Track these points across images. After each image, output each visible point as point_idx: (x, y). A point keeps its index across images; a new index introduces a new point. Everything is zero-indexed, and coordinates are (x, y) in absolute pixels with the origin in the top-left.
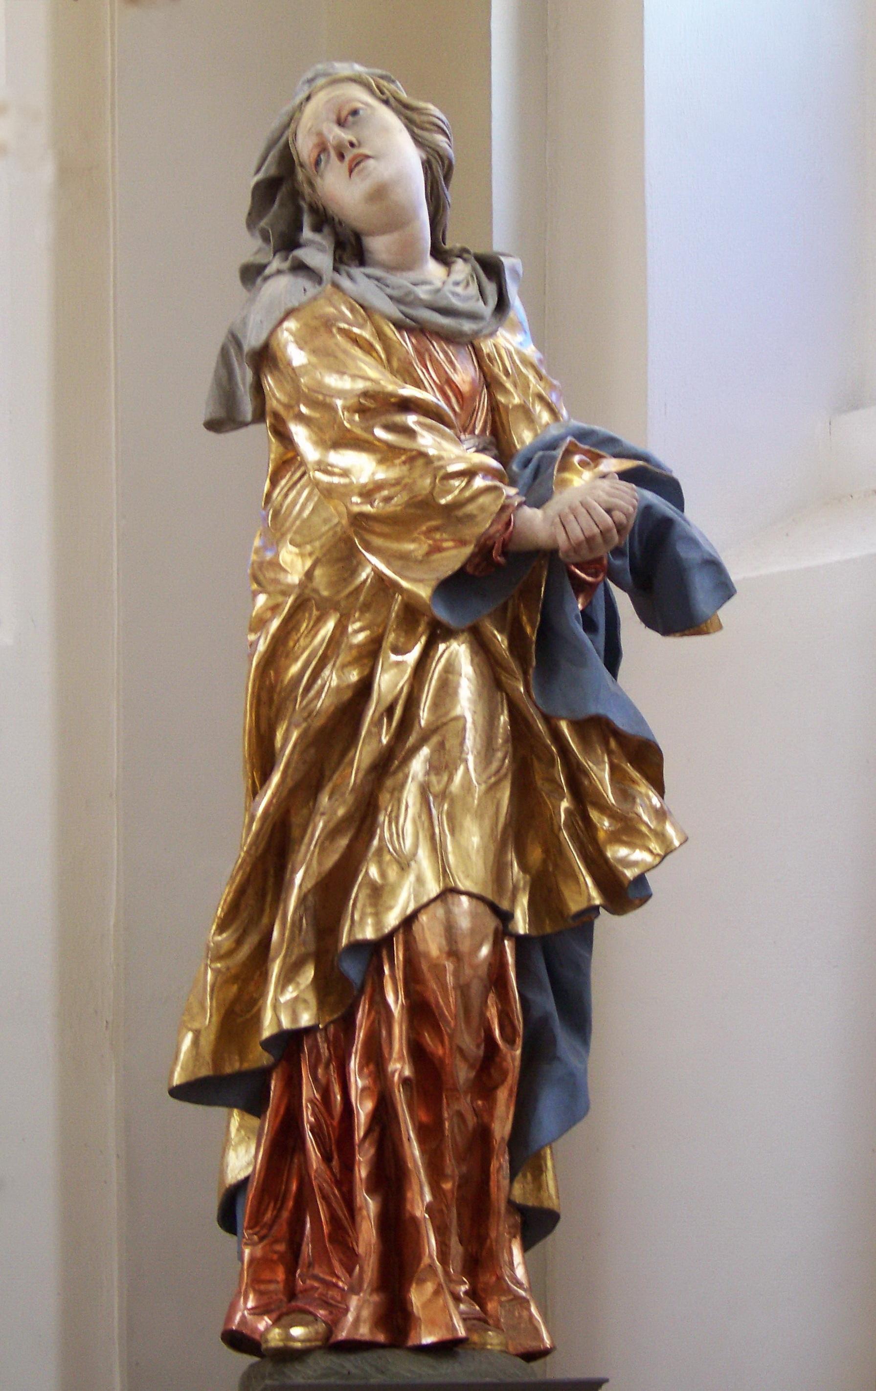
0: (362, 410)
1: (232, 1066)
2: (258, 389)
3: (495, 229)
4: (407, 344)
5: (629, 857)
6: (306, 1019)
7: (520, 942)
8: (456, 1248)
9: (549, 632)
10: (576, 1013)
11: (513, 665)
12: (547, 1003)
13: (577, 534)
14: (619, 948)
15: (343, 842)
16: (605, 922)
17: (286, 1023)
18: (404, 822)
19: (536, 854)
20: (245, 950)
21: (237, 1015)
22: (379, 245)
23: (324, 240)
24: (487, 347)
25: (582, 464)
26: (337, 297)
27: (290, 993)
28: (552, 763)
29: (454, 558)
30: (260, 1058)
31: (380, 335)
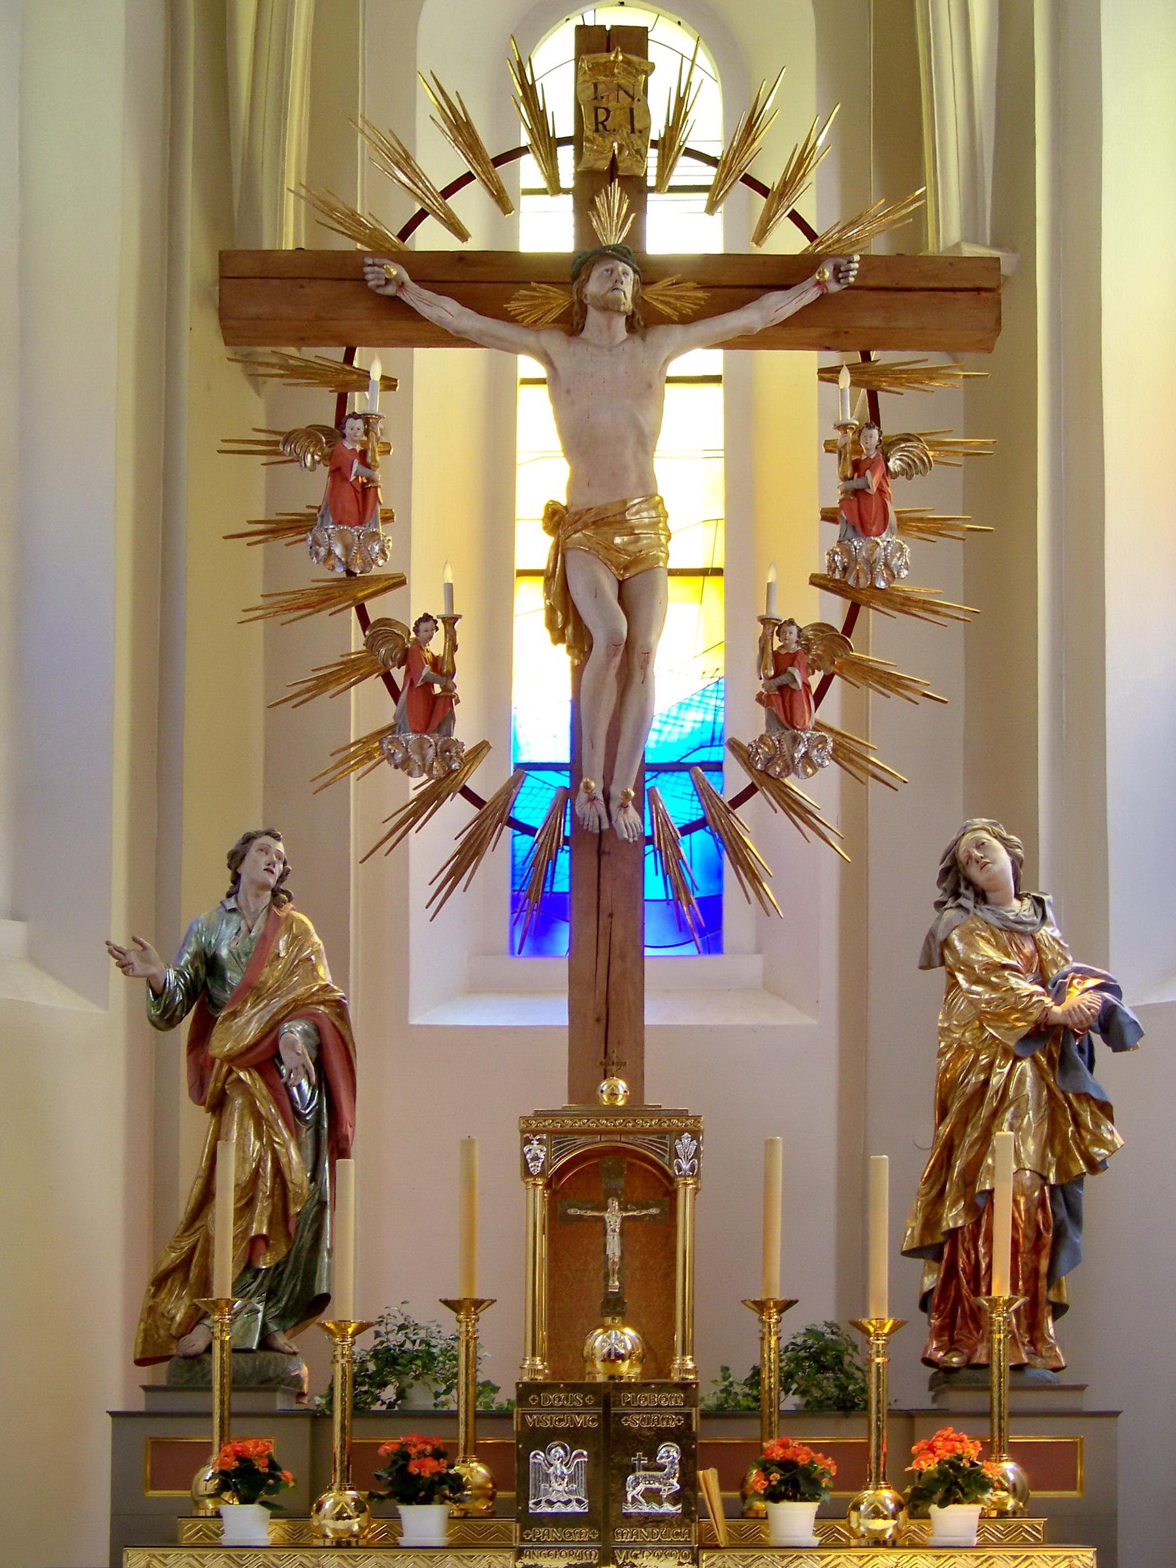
0: (986, 970)
1: (928, 1241)
2: (942, 955)
3: (1040, 744)
4: (1005, 936)
5: (1099, 1152)
6: (960, 1223)
7: (1052, 1188)
8: (1024, 1322)
9: (1064, 1056)
10: (1075, 1214)
11: (1049, 1071)
12: (1063, 1213)
13: (1076, 1019)
14: (1093, 1192)
15: (977, 1148)
16: (1088, 1178)
17: (951, 1225)
18: (1004, 1133)
19: (1058, 1148)
20: (933, 1193)
21: (931, 1222)
22: (990, 896)
23: (970, 893)
24: (1038, 936)
25: (1079, 983)
26: (975, 919)
27: (954, 1212)
28: (1065, 1111)
29: (1023, 1027)
30: (940, 1239)
31: (993, 934)
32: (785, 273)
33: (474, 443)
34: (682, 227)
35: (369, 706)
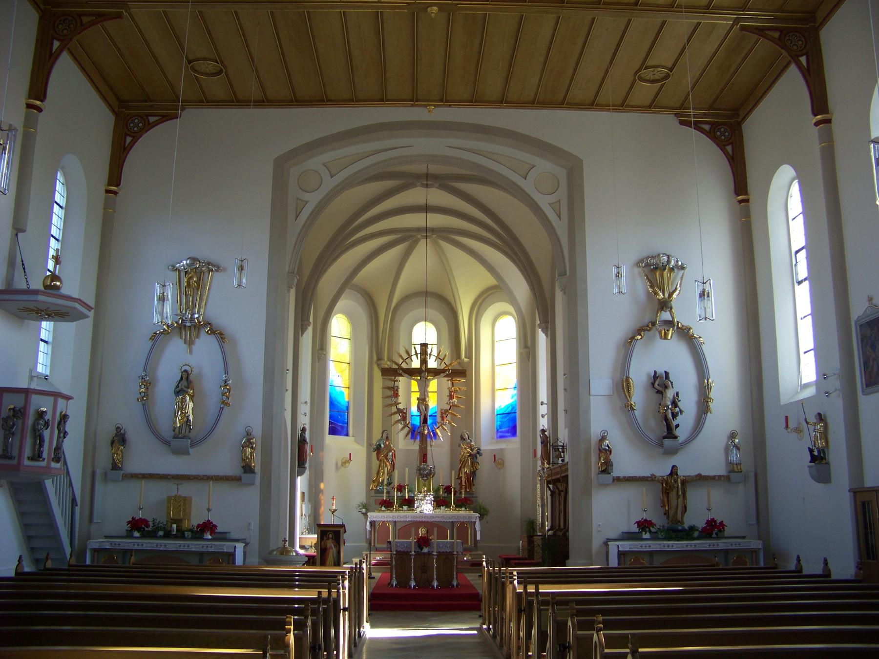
32: (443, 371)
33: (410, 392)
34: (432, 364)
35: (398, 417)
